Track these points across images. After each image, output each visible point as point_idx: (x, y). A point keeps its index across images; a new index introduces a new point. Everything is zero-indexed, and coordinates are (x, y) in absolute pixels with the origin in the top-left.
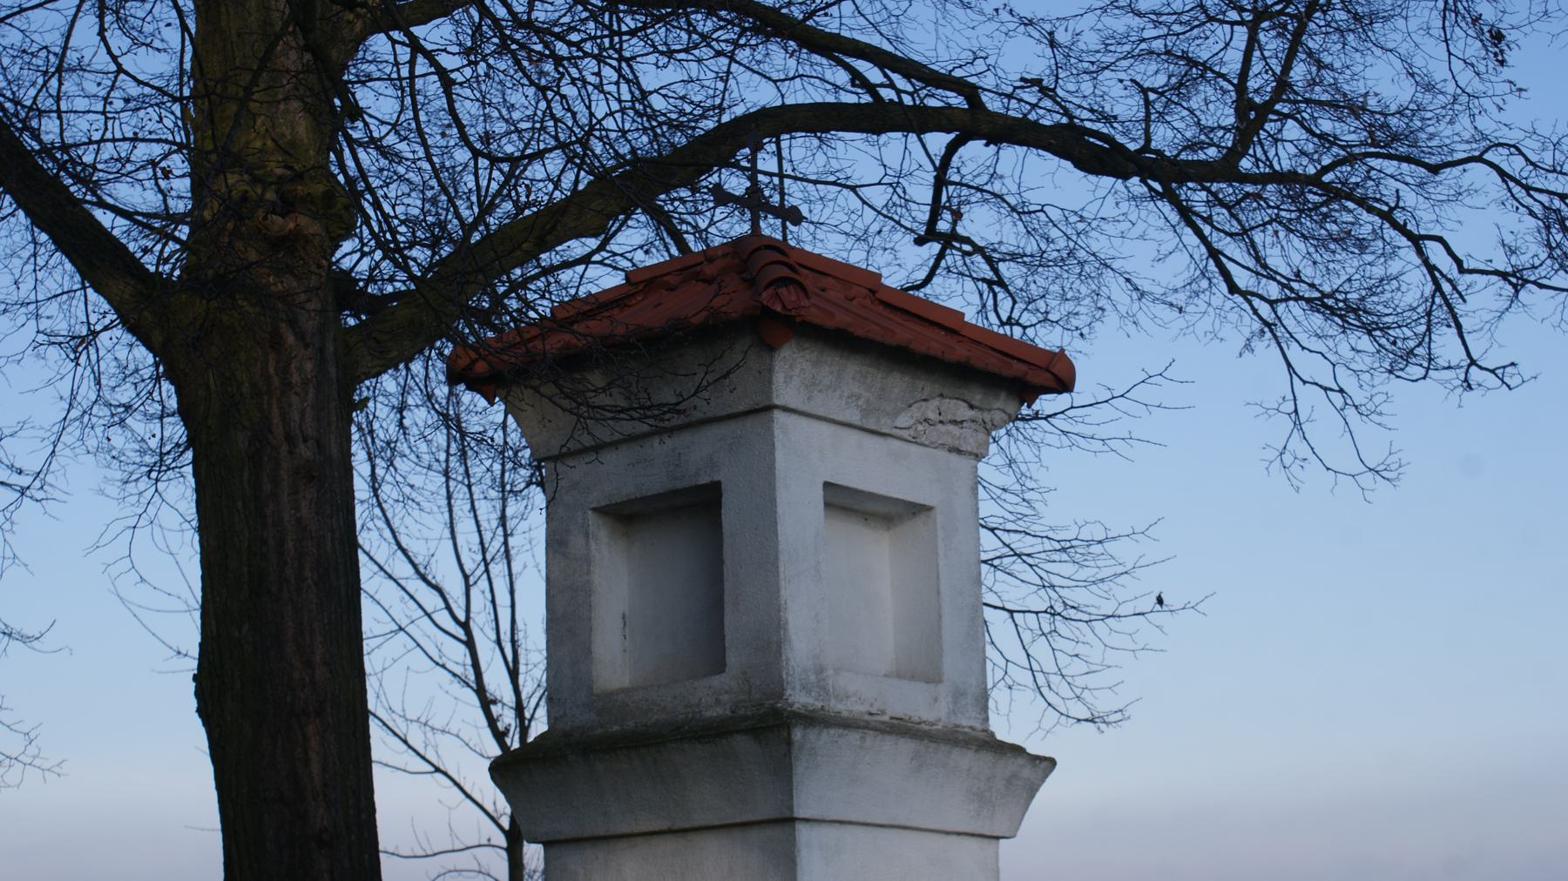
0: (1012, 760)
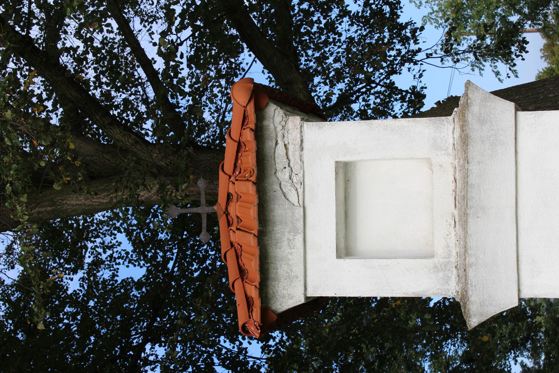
0: (470, 126)
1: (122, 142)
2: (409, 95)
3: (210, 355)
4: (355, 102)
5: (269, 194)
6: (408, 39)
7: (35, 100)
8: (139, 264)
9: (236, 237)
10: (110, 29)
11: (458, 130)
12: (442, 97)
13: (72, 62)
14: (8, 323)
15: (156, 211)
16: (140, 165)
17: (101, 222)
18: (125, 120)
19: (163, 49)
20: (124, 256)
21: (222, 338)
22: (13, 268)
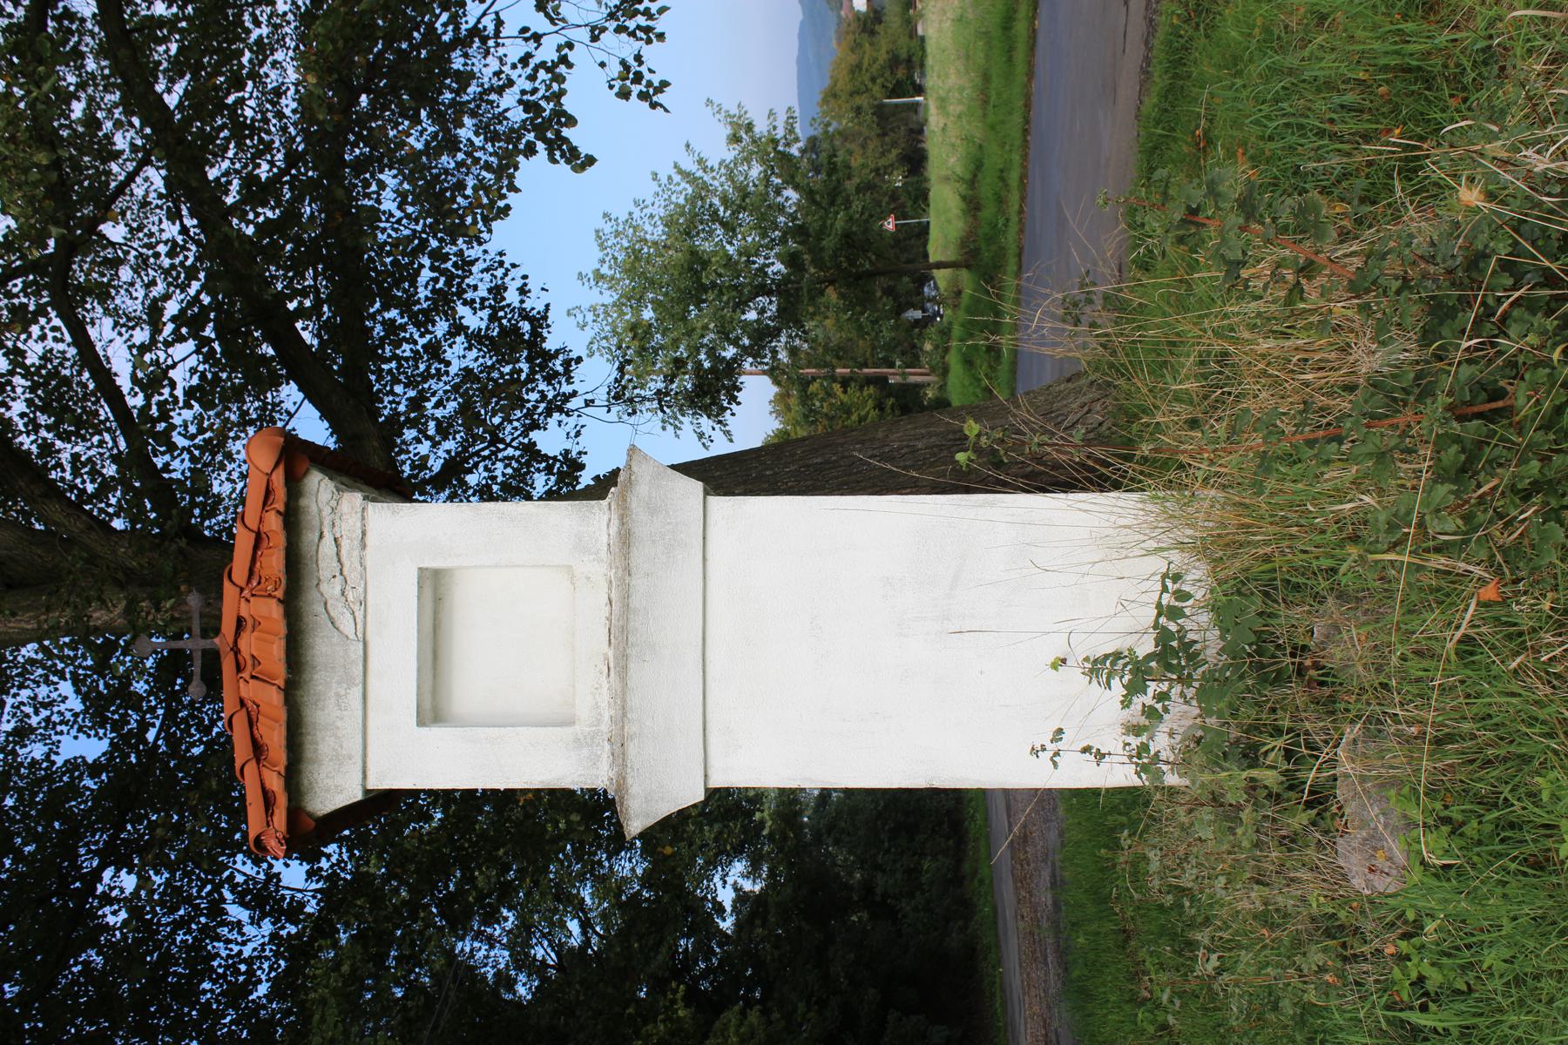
2: (558, 465)
4: (470, 471)
5: (305, 620)
6: (557, 374)
8: (97, 734)
9: (250, 690)
11: (615, 522)
12: (603, 470)
17: (32, 662)
21: (240, 857)
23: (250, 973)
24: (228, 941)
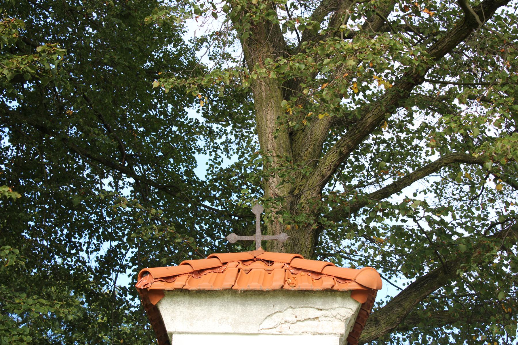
1: (324, 163)
3: (120, 239)
5: (271, 300)
7: (364, 84)
8: (208, 174)
9: (232, 268)
10: (430, 153)
13: (399, 119)
14: (160, 53)
15: (258, 191)
16: (302, 179)
18: (344, 166)
19: (410, 203)
20: (217, 160)
21: (136, 250)
22: (210, 59)
23: (70, 255)
24: (89, 243)
